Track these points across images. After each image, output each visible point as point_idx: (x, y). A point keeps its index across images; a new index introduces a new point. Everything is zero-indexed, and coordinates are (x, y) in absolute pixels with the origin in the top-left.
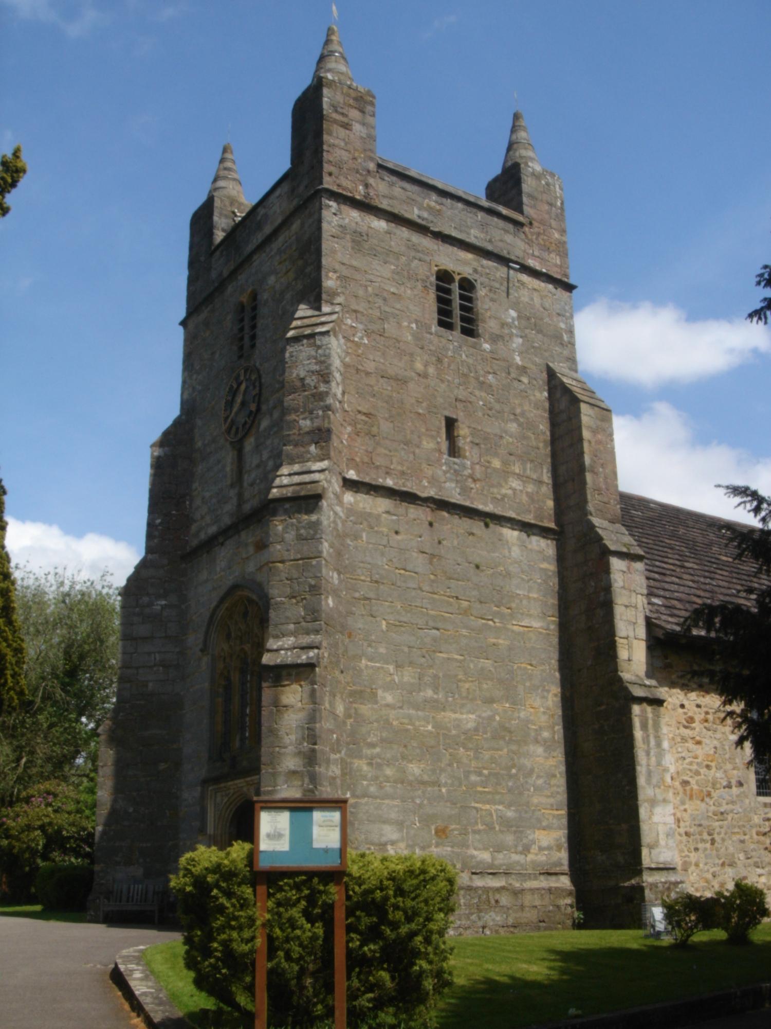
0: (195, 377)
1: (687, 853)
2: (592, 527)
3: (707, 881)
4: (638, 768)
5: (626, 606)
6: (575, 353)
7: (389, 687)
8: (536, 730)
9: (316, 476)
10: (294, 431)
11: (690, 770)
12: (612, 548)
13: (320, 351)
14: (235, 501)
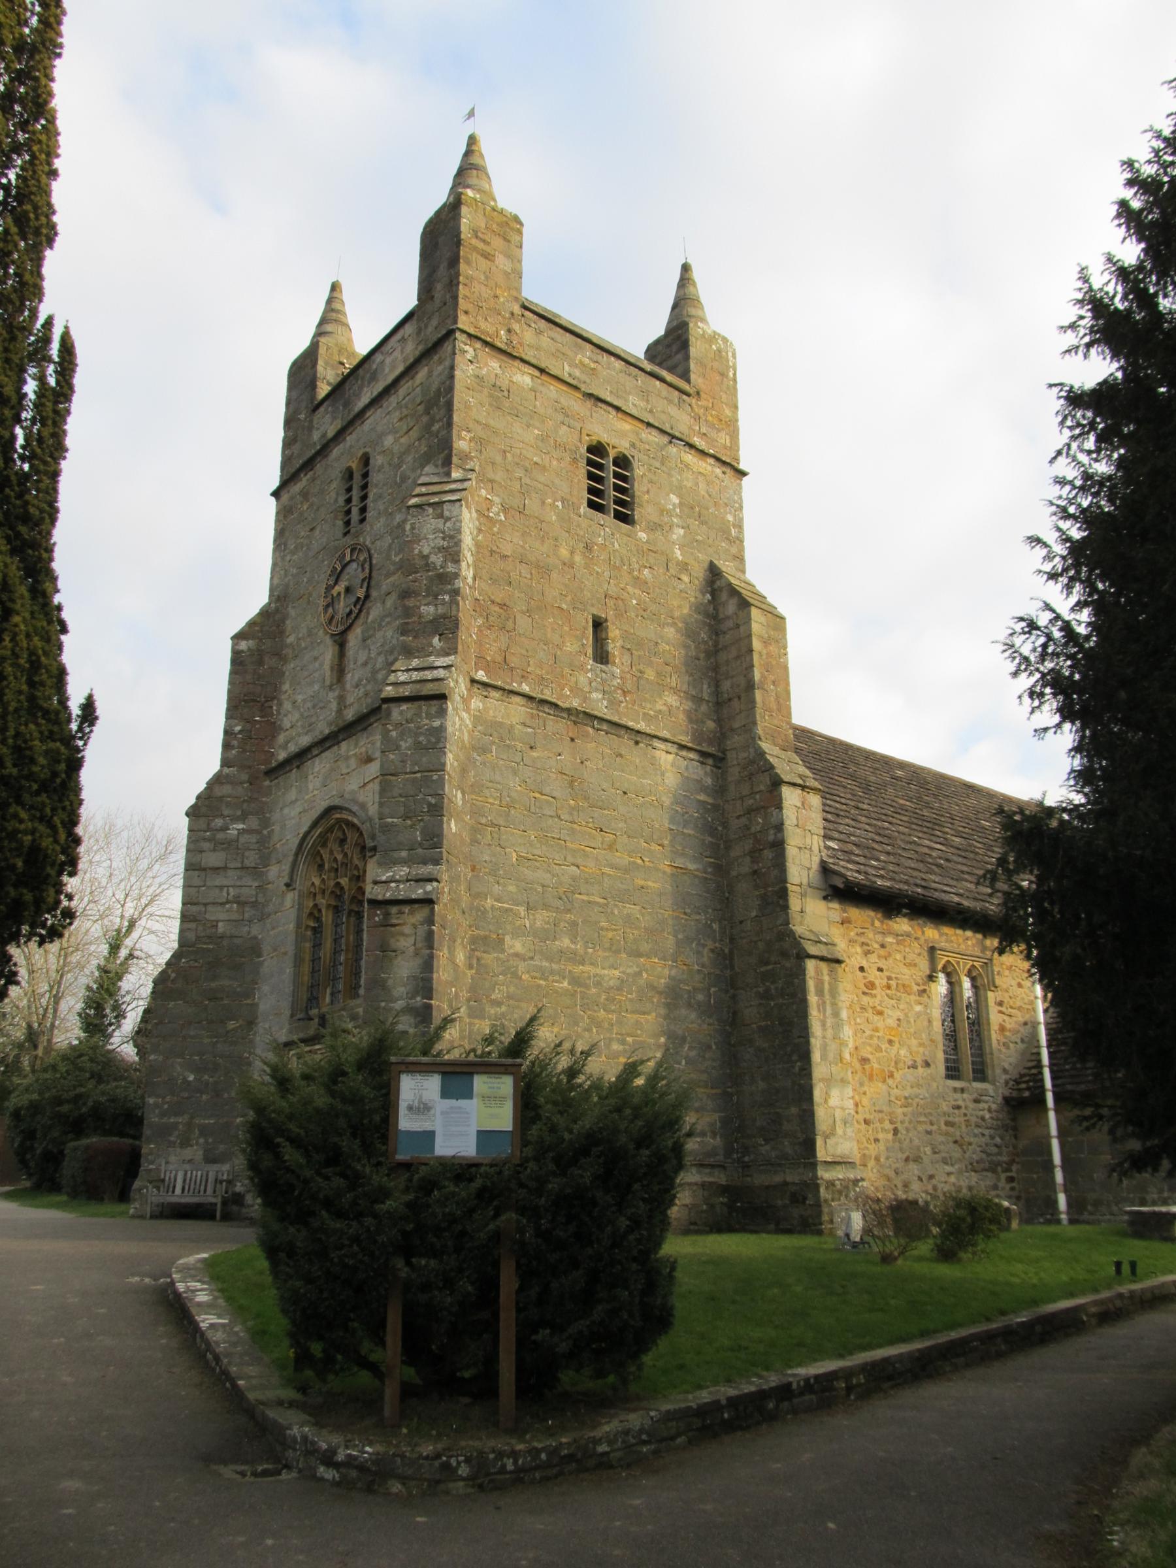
0: (288, 558)
1: (866, 1144)
2: (762, 754)
3: (889, 1179)
4: (812, 1040)
5: (800, 848)
6: (743, 550)
7: (517, 933)
8: (689, 992)
9: (441, 673)
10: (415, 619)
11: (870, 1045)
12: (786, 778)
13: (448, 524)
14: (334, 706)
